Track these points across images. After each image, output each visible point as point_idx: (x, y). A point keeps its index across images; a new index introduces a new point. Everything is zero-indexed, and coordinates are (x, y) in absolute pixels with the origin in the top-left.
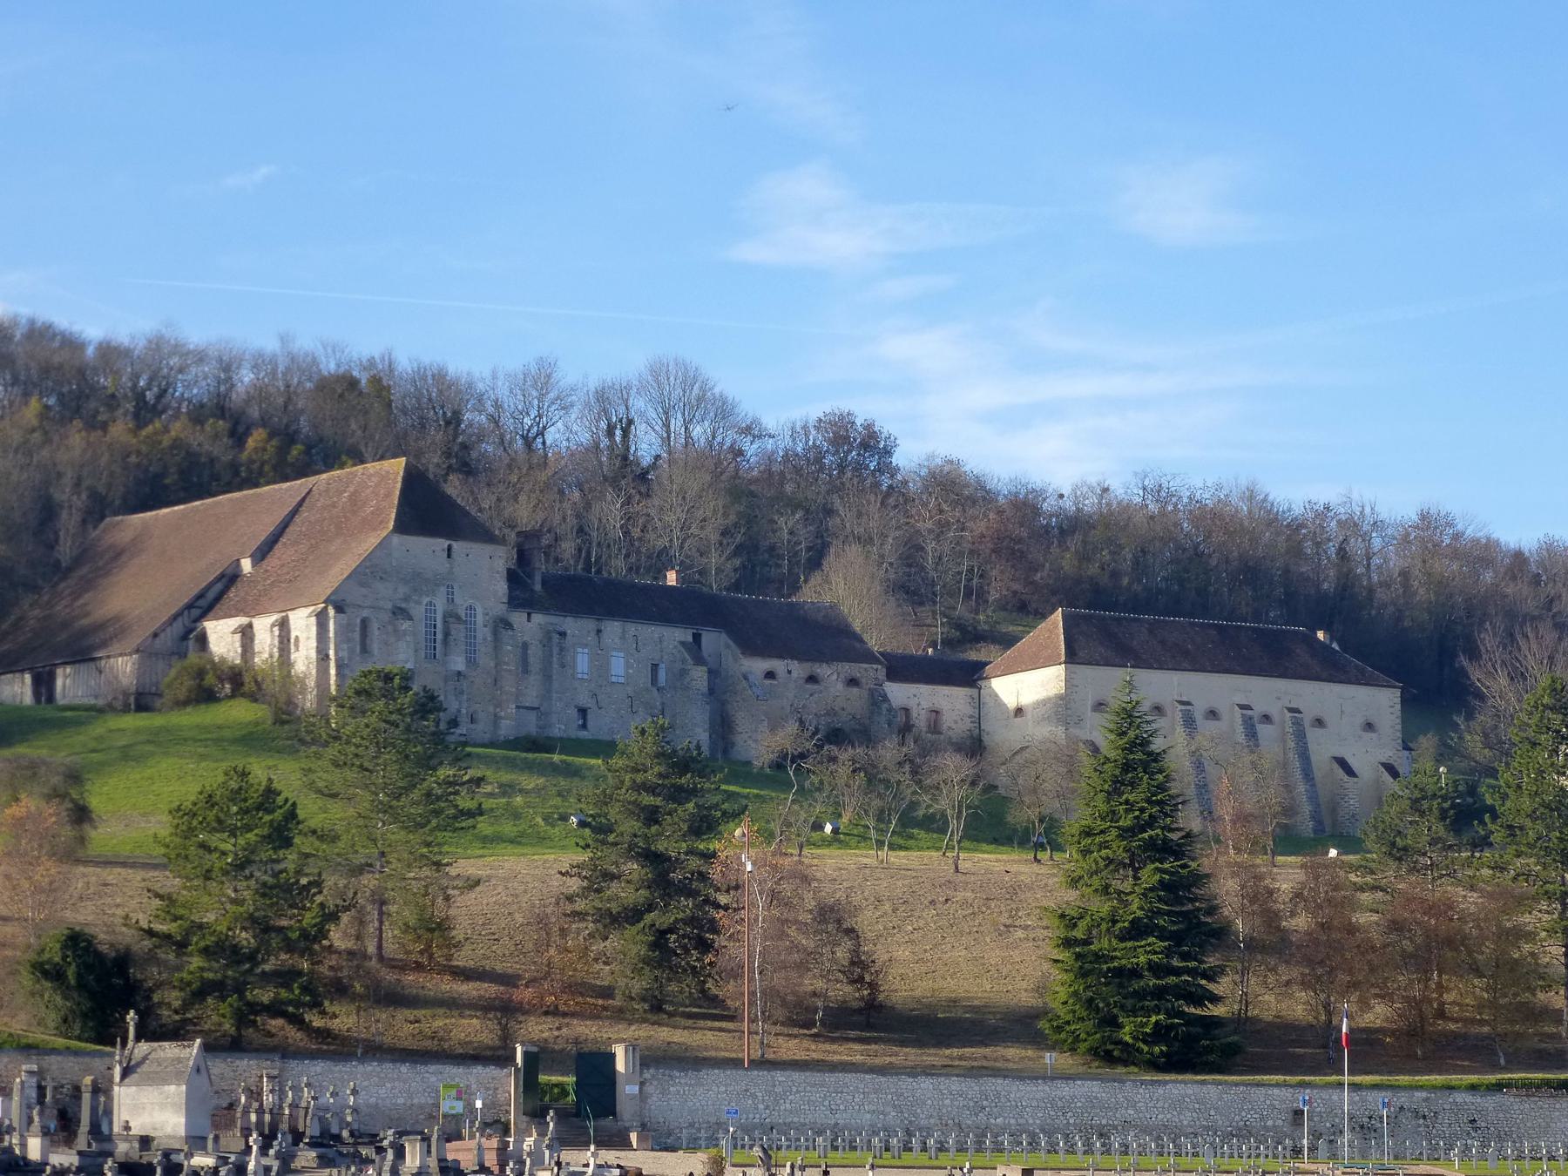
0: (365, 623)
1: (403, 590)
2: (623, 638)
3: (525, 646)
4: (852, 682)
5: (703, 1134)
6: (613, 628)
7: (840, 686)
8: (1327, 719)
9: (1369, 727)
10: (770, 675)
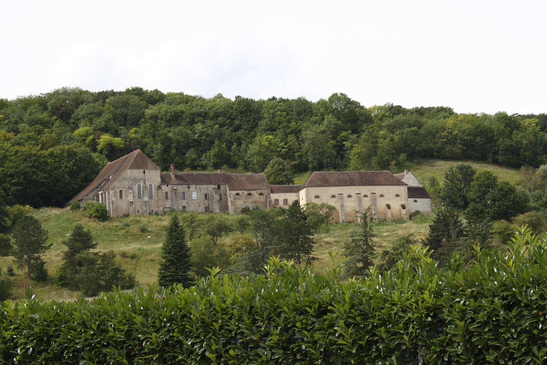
0: (121, 191)
1: (131, 183)
2: (196, 188)
3: (167, 193)
4: (261, 194)
5: (173, 145)
6: (193, 187)
7: (257, 195)
8: (384, 195)
9: (397, 196)
10: (238, 194)
